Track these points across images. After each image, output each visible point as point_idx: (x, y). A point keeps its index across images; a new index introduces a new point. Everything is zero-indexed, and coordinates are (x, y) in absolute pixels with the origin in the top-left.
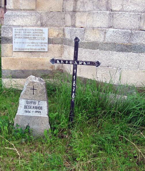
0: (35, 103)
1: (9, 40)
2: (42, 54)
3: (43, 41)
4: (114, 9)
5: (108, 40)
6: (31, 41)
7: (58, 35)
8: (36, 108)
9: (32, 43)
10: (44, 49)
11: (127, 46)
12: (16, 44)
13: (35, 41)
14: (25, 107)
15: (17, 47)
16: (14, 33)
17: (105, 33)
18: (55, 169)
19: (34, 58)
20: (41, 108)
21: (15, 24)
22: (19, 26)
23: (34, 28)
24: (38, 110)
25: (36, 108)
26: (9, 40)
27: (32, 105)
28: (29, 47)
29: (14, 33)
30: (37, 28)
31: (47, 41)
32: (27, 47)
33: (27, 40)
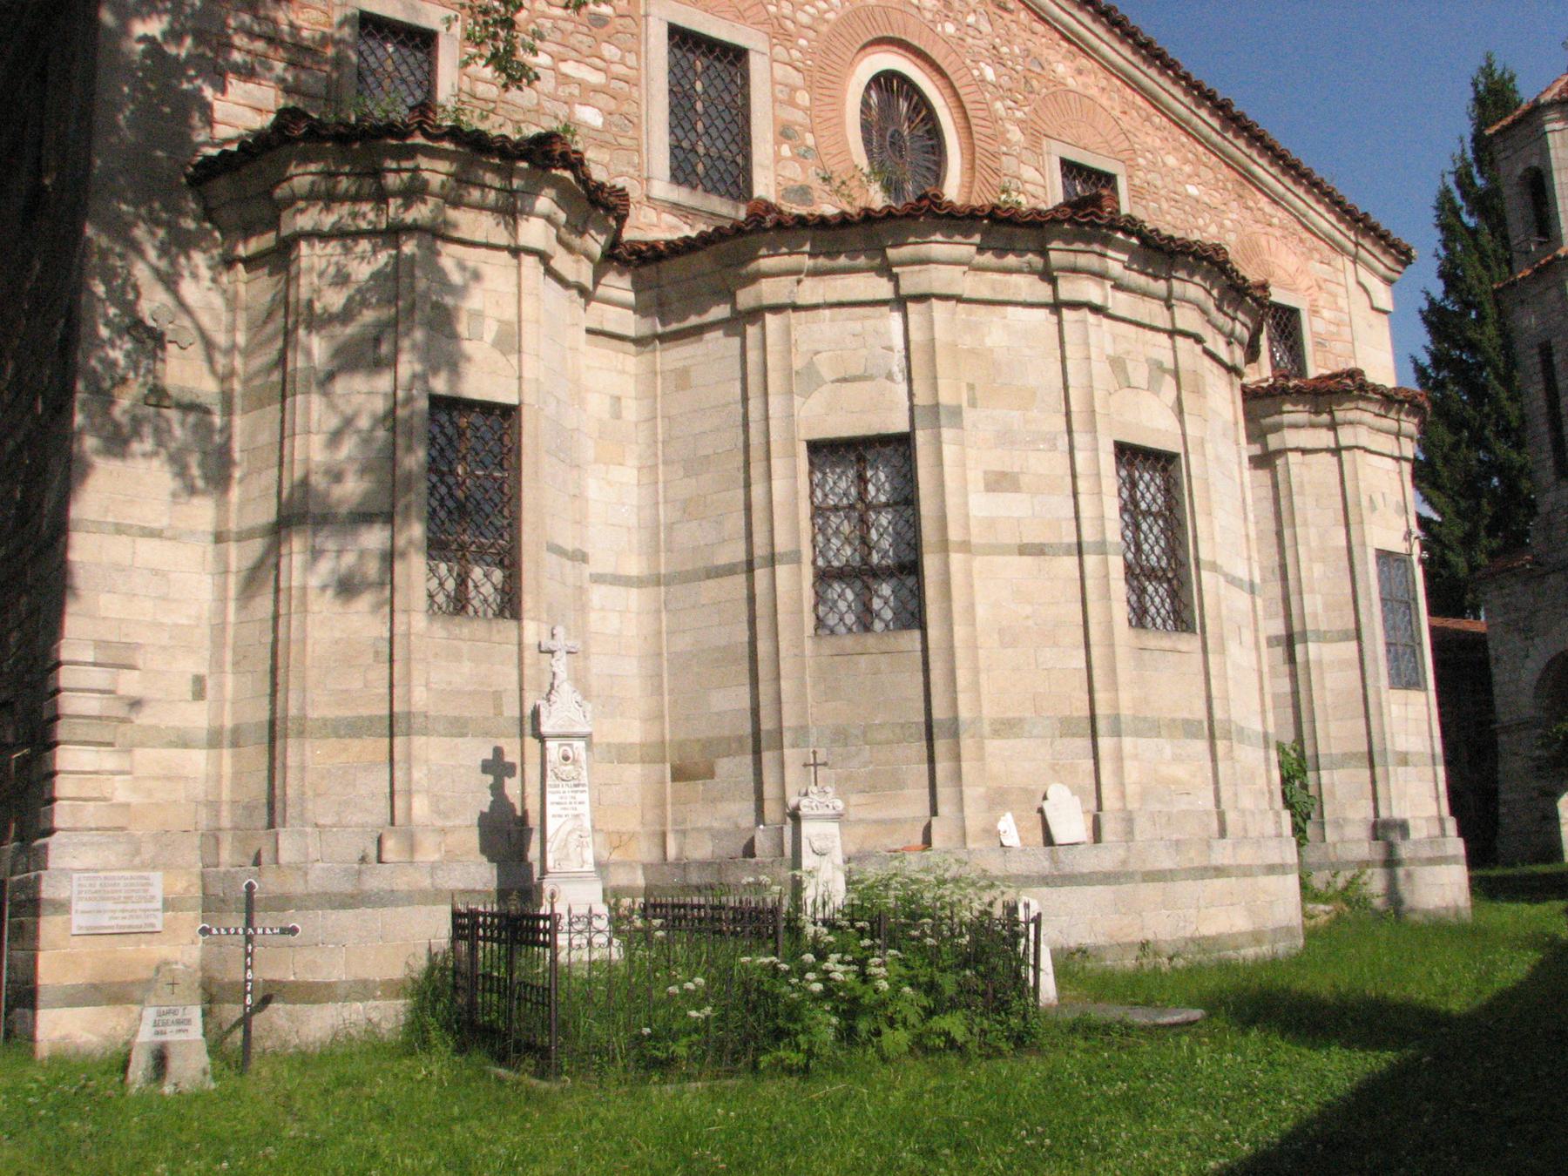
0: (175, 1013)
1: (62, 907)
2: (148, 937)
3: (150, 906)
4: (321, 822)
5: (314, 887)
6: (120, 907)
7: (187, 889)
8: (179, 1022)
9: (123, 911)
10: (152, 925)
11: (352, 897)
12: (79, 920)
13: (130, 906)
14: (156, 1024)
15: (83, 924)
16: (75, 889)
17: (306, 874)
18: (804, 802)
19: (127, 949)
20: (189, 1022)
21: (77, 864)
22: (87, 870)
23: (127, 874)
24: (182, 1027)
25: (179, 1022)
26: (62, 907)
27: (170, 1017)
28: (113, 923)
29: (75, 889)
30: (135, 874)
31: (159, 905)
32: (106, 921)
33: (110, 905)
